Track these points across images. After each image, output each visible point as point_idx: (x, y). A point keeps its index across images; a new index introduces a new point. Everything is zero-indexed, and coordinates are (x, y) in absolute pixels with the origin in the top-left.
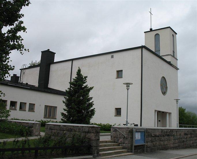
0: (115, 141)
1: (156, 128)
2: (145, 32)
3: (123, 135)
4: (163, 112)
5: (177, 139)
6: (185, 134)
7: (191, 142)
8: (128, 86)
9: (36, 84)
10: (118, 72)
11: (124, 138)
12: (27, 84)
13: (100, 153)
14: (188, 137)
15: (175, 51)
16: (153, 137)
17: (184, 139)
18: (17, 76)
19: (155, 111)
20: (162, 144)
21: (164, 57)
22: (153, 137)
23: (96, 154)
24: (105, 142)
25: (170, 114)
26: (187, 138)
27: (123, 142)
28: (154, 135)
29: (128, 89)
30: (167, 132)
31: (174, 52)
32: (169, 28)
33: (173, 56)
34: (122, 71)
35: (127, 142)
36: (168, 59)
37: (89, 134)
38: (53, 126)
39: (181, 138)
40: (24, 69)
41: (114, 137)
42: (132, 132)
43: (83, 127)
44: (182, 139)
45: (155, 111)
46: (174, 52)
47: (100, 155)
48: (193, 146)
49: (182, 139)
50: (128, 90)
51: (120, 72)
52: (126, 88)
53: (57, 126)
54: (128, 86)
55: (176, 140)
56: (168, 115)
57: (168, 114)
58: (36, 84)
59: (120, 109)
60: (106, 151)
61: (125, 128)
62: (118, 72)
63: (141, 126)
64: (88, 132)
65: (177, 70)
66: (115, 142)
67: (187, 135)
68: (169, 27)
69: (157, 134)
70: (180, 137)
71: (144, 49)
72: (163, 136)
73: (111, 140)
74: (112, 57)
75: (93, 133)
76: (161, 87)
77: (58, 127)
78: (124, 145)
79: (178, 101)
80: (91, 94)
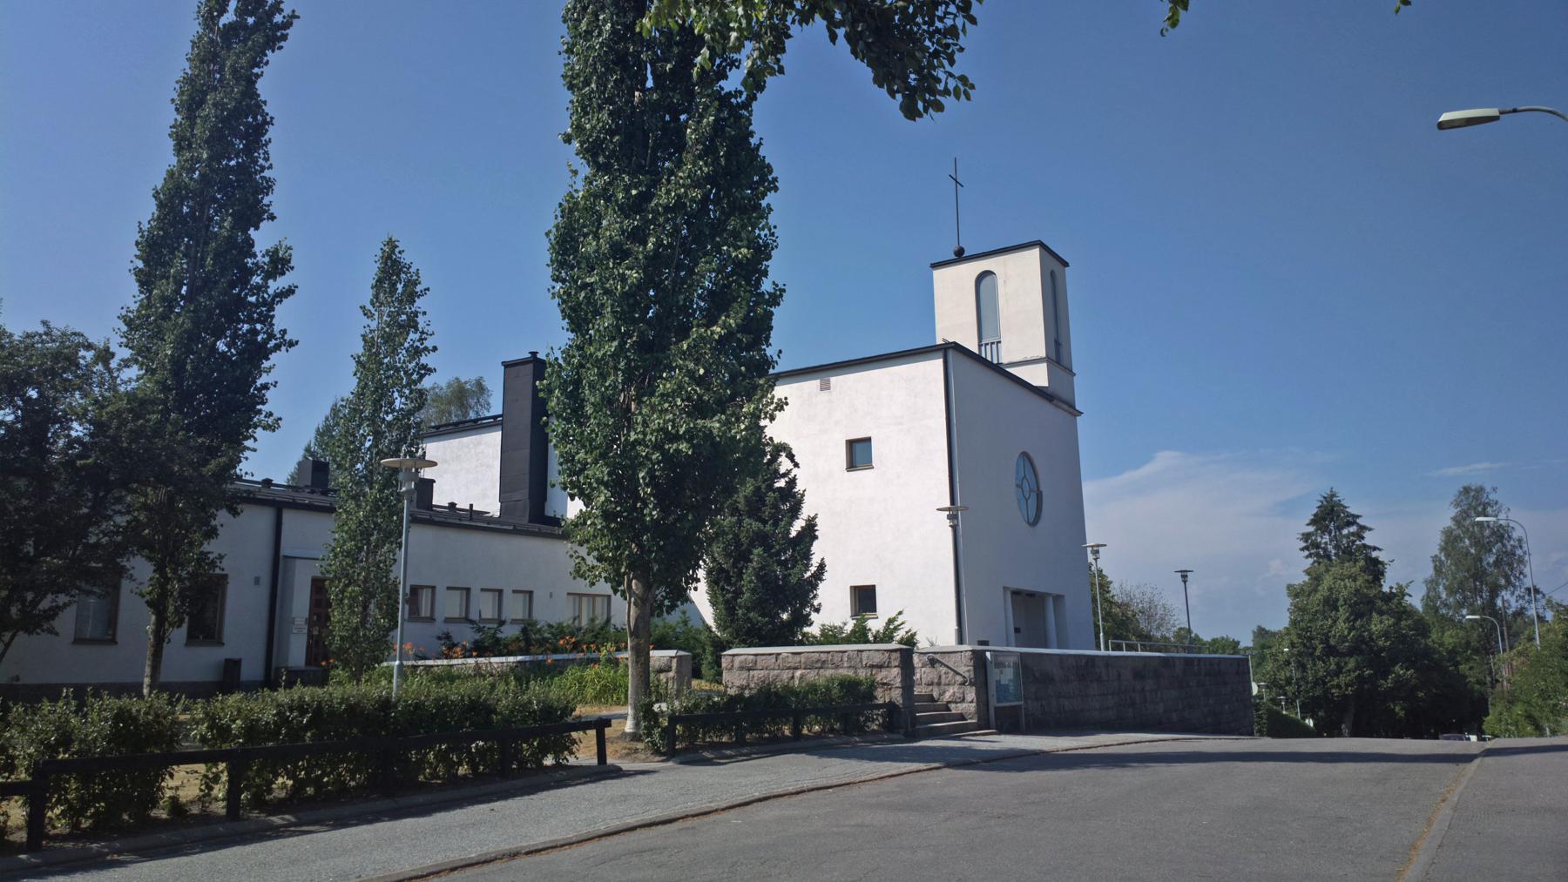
4: (1031, 595)
8: (1184, 577)
9: (491, 505)
10: (851, 444)
15: (1063, 341)
19: (1005, 588)
25: (1058, 598)
27: (960, 698)
34: (869, 440)
37: (884, 673)
45: (1005, 588)
51: (858, 446)
54: (1184, 577)
56: (1050, 603)
57: (1051, 599)
58: (491, 505)
59: (874, 586)
61: (961, 652)
62: (851, 444)
65: (1075, 416)
71: (951, 354)
77: (774, 660)
78: (964, 705)
79: (1186, 576)
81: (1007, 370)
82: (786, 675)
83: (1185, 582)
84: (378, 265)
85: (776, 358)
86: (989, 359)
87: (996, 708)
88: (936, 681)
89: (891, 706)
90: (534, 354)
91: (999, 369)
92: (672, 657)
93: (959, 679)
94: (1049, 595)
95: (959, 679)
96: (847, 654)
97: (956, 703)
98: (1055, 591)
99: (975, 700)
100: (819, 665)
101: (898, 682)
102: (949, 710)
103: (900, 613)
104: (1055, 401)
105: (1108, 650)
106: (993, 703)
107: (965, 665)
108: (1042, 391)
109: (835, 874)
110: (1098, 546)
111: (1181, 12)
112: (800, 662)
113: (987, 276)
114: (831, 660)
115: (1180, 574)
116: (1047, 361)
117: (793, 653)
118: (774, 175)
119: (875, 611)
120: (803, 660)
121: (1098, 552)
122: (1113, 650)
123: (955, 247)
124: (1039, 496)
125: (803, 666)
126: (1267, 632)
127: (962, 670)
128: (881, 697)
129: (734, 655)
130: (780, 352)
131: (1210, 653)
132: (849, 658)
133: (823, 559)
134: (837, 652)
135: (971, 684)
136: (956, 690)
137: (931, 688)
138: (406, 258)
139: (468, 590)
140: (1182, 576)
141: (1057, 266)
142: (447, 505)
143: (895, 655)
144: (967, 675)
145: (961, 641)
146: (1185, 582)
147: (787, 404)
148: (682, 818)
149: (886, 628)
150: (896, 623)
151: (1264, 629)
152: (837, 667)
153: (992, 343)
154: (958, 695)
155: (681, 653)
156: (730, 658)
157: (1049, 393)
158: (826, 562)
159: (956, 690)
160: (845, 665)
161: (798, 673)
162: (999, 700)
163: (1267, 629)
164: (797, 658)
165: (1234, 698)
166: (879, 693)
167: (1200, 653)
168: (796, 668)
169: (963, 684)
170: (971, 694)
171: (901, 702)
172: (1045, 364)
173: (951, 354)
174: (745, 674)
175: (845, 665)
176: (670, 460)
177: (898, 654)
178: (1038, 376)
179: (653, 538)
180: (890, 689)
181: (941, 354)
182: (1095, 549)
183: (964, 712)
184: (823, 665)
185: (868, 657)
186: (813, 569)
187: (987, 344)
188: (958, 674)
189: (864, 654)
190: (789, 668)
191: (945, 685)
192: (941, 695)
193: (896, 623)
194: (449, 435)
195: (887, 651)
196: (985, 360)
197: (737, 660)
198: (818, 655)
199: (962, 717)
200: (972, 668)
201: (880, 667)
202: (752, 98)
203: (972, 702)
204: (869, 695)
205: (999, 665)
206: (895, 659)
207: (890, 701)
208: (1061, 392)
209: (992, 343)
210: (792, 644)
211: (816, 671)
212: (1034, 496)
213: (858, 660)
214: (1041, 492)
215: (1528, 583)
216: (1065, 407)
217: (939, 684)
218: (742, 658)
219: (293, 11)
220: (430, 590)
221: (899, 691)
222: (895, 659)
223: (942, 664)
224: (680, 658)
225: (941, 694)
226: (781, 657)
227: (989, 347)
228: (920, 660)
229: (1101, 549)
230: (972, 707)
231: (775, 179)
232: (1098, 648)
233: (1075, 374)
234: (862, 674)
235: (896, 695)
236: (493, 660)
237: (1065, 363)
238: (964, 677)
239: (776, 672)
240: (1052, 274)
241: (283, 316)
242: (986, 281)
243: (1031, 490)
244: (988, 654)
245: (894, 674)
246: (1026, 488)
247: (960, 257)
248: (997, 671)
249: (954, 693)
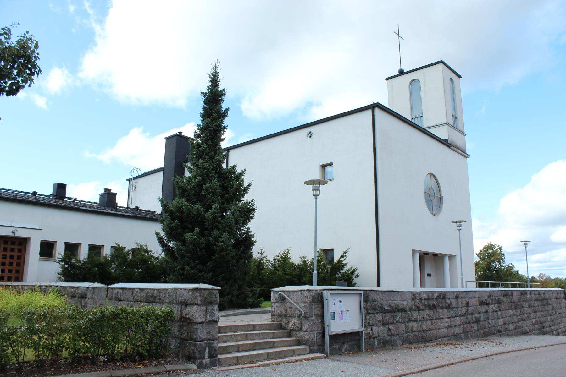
0: (281, 325)
1: (418, 289)
2: (387, 79)
3: (297, 309)
4: (436, 255)
5: (461, 316)
6: (482, 303)
7: (501, 321)
8: (526, 244)
11: (299, 317)
12: (137, 208)
13: (219, 356)
14: (491, 310)
16: (388, 311)
17: (477, 315)
18: (112, 191)
19: (414, 251)
20: (414, 329)
21: (431, 131)
22: (388, 311)
23: (207, 360)
24: (252, 328)
25: (452, 257)
26: (486, 312)
27: (298, 328)
28: (390, 306)
29: (316, 196)
30: (428, 299)
31: (455, 117)
32: (441, 64)
33: (454, 127)
35: (306, 326)
36: (442, 133)
37: (188, 309)
38: (121, 291)
39: (470, 312)
40: (139, 177)
41: (279, 316)
42: (322, 302)
43: (176, 289)
44: (472, 314)
45: (414, 251)
46: (455, 117)
47: (220, 363)
48: (507, 330)
49: (472, 314)
50: (316, 199)
52: (312, 193)
53: (129, 291)
54: (526, 244)
55: (458, 318)
56: (447, 260)
60: (243, 351)
61: (301, 291)
63: (378, 285)
64: (185, 304)
66: (280, 327)
67: (488, 304)
68: (441, 62)
69: (405, 303)
70: (467, 311)
71: (377, 110)
72: (419, 309)
73: (272, 321)
74: (310, 135)
75: (197, 304)
76: (426, 199)
77: (131, 294)
78: (302, 333)
79: (527, 244)
80: (520, 273)
81: (428, 130)
88: (283, 313)
94: (446, 255)
117: (140, 289)
131: (365, 339)
136: (296, 321)
137: (280, 318)
141: (455, 77)
142: (135, 208)
146: (526, 247)
154: (297, 325)
159: (296, 321)
165: (554, 312)
167: (268, 354)
191: (289, 317)
217: (285, 316)
218: (115, 291)
225: (287, 324)
228: (274, 297)
232: (463, 287)
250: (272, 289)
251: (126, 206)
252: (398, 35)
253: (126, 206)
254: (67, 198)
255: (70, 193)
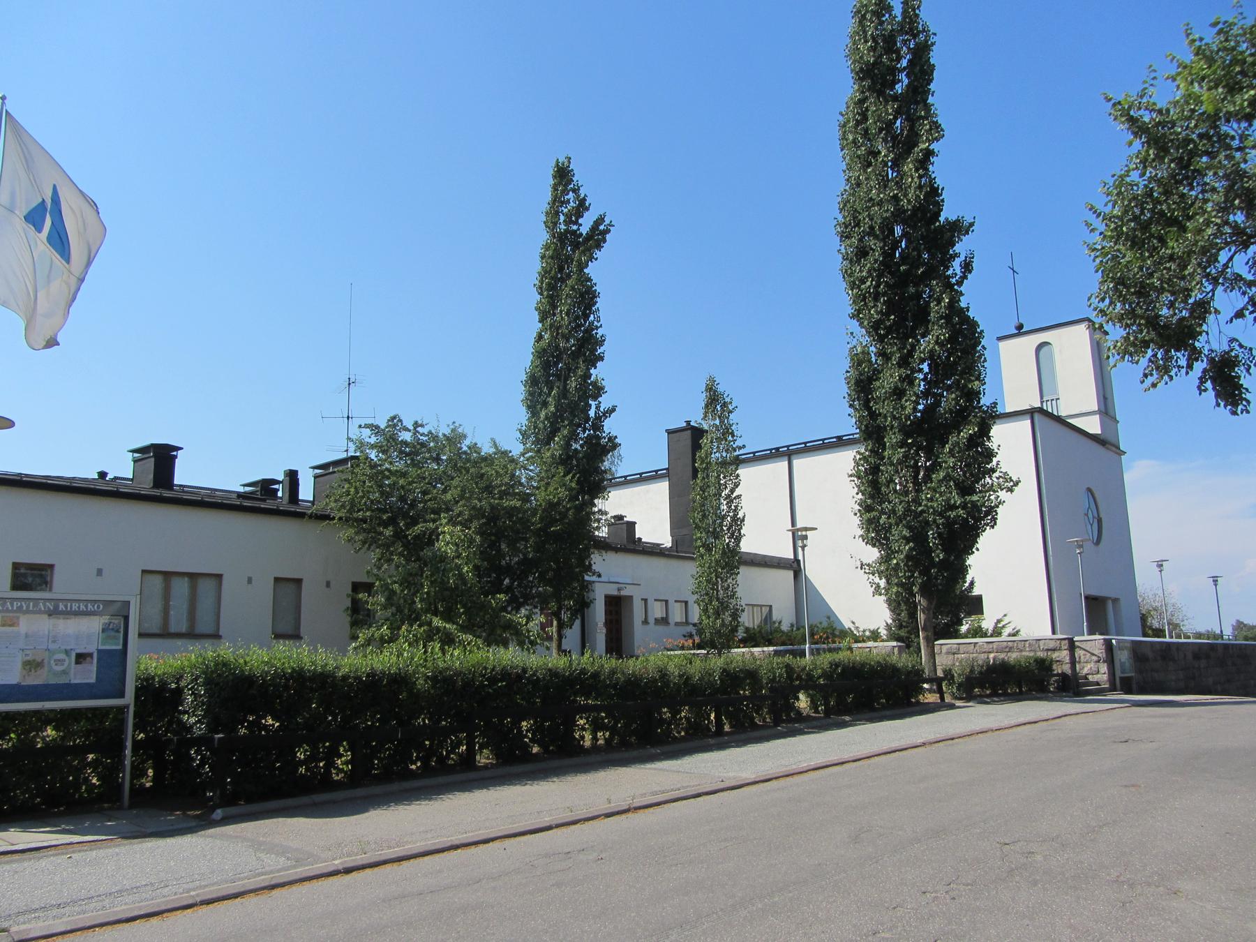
8: (1215, 582)
15: (1108, 396)
25: (1115, 601)
29: (1161, 571)
54: (1215, 582)
56: (1110, 605)
57: (1110, 601)
58: (666, 541)
71: (1037, 416)
77: (973, 647)
78: (1099, 676)
79: (1217, 581)
81: (1068, 421)
82: (983, 656)
83: (1216, 585)
84: (704, 394)
85: (996, 450)
86: (1050, 410)
87: (1121, 679)
89: (1063, 676)
90: (688, 422)
91: (1059, 420)
92: (894, 647)
93: (1095, 658)
94: (1110, 598)
95: (1095, 658)
96: (1028, 642)
97: (1093, 674)
98: (1113, 595)
99: (1107, 672)
100: (1007, 650)
101: (1067, 659)
102: (1087, 679)
103: (1005, 615)
104: (1107, 446)
105: (1172, 637)
106: (1118, 674)
107: (1099, 649)
108: (1098, 438)
109: (686, 898)
110: (1162, 561)
111: (1170, 80)
112: (993, 648)
113: (1044, 346)
114: (1017, 646)
115: (1212, 579)
116: (1100, 414)
117: (987, 642)
118: (981, 328)
119: (983, 614)
120: (995, 647)
121: (1162, 565)
122: (1176, 638)
123: (1015, 323)
124: (1100, 521)
125: (995, 651)
126: (1245, 625)
127: (1096, 652)
128: (1057, 669)
129: (941, 645)
130: (999, 446)
132: (1030, 645)
133: (973, 578)
134: (1020, 641)
135: (1104, 662)
138: (720, 389)
139: (666, 601)
140: (1213, 581)
143: (1063, 642)
144: (1100, 655)
145: (1054, 632)
146: (1216, 585)
147: (1020, 481)
148: (776, 778)
149: (996, 627)
150: (1003, 623)
151: (1242, 623)
152: (1021, 651)
153: (1052, 400)
155: (899, 644)
156: (939, 647)
157: (1101, 438)
158: (975, 580)
160: (1027, 649)
161: (992, 656)
162: (1122, 673)
163: (1245, 622)
164: (991, 646)
166: (1054, 667)
168: (990, 652)
169: (1099, 661)
170: (1104, 668)
171: (1070, 672)
172: (1098, 416)
173: (1037, 416)
174: (951, 657)
175: (1027, 649)
176: (949, 524)
177: (1067, 641)
178: (1093, 425)
179: (939, 571)
180: (1062, 664)
181: (1028, 416)
182: (1159, 563)
183: (1099, 680)
184: (1011, 649)
185: (1044, 644)
186: (967, 585)
187: (1048, 400)
188: (1093, 654)
189: (1041, 642)
190: (984, 652)
192: (1081, 669)
193: (1003, 623)
194: (618, 487)
195: (1058, 639)
196: (1047, 411)
197: (944, 649)
198: (1005, 643)
199: (1098, 684)
200: (1104, 651)
201: (1054, 650)
202: (964, 277)
203: (1105, 674)
204: (1049, 668)
205: (1120, 649)
206: (1065, 645)
207: (1062, 672)
208: (1110, 438)
209: (1052, 400)
210: (956, 637)
211: (1006, 654)
212: (1096, 521)
213: (1037, 646)
214: (1101, 519)
215: (1151, 389)
216: (1114, 449)
219: (611, 222)
220: (664, 603)
221: (1069, 666)
222: (1065, 645)
223: (1081, 648)
224: (899, 647)
226: (978, 645)
227: (1049, 403)
229: (1164, 563)
230: (1105, 677)
231: (982, 331)
233: (1118, 422)
234: (1041, 654)
235: (1066, 668)
236: (756, 650)
237: (1111, 413)
238: (1099, 657)
239: (974, 655)
240: (1098, 343)
241: (609, 426)
242: (1044, 350)
243: (1094, 517)
244: (1114, 641)
245: (1064, 655)
246: (1090, 515)
247: (1020, 331)
248: (1119, 652)
249: (1091, 668)
250: (935, 643)
251: (746, 546)
252: (1013, 269)
253: (746, 546)
254: (177, 485)
255: (185, 474)
